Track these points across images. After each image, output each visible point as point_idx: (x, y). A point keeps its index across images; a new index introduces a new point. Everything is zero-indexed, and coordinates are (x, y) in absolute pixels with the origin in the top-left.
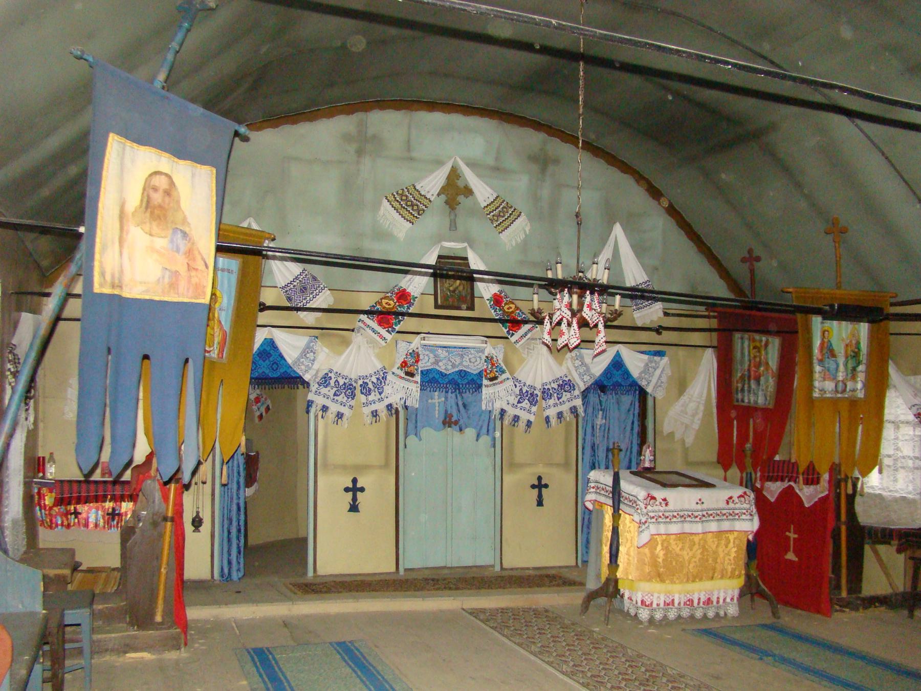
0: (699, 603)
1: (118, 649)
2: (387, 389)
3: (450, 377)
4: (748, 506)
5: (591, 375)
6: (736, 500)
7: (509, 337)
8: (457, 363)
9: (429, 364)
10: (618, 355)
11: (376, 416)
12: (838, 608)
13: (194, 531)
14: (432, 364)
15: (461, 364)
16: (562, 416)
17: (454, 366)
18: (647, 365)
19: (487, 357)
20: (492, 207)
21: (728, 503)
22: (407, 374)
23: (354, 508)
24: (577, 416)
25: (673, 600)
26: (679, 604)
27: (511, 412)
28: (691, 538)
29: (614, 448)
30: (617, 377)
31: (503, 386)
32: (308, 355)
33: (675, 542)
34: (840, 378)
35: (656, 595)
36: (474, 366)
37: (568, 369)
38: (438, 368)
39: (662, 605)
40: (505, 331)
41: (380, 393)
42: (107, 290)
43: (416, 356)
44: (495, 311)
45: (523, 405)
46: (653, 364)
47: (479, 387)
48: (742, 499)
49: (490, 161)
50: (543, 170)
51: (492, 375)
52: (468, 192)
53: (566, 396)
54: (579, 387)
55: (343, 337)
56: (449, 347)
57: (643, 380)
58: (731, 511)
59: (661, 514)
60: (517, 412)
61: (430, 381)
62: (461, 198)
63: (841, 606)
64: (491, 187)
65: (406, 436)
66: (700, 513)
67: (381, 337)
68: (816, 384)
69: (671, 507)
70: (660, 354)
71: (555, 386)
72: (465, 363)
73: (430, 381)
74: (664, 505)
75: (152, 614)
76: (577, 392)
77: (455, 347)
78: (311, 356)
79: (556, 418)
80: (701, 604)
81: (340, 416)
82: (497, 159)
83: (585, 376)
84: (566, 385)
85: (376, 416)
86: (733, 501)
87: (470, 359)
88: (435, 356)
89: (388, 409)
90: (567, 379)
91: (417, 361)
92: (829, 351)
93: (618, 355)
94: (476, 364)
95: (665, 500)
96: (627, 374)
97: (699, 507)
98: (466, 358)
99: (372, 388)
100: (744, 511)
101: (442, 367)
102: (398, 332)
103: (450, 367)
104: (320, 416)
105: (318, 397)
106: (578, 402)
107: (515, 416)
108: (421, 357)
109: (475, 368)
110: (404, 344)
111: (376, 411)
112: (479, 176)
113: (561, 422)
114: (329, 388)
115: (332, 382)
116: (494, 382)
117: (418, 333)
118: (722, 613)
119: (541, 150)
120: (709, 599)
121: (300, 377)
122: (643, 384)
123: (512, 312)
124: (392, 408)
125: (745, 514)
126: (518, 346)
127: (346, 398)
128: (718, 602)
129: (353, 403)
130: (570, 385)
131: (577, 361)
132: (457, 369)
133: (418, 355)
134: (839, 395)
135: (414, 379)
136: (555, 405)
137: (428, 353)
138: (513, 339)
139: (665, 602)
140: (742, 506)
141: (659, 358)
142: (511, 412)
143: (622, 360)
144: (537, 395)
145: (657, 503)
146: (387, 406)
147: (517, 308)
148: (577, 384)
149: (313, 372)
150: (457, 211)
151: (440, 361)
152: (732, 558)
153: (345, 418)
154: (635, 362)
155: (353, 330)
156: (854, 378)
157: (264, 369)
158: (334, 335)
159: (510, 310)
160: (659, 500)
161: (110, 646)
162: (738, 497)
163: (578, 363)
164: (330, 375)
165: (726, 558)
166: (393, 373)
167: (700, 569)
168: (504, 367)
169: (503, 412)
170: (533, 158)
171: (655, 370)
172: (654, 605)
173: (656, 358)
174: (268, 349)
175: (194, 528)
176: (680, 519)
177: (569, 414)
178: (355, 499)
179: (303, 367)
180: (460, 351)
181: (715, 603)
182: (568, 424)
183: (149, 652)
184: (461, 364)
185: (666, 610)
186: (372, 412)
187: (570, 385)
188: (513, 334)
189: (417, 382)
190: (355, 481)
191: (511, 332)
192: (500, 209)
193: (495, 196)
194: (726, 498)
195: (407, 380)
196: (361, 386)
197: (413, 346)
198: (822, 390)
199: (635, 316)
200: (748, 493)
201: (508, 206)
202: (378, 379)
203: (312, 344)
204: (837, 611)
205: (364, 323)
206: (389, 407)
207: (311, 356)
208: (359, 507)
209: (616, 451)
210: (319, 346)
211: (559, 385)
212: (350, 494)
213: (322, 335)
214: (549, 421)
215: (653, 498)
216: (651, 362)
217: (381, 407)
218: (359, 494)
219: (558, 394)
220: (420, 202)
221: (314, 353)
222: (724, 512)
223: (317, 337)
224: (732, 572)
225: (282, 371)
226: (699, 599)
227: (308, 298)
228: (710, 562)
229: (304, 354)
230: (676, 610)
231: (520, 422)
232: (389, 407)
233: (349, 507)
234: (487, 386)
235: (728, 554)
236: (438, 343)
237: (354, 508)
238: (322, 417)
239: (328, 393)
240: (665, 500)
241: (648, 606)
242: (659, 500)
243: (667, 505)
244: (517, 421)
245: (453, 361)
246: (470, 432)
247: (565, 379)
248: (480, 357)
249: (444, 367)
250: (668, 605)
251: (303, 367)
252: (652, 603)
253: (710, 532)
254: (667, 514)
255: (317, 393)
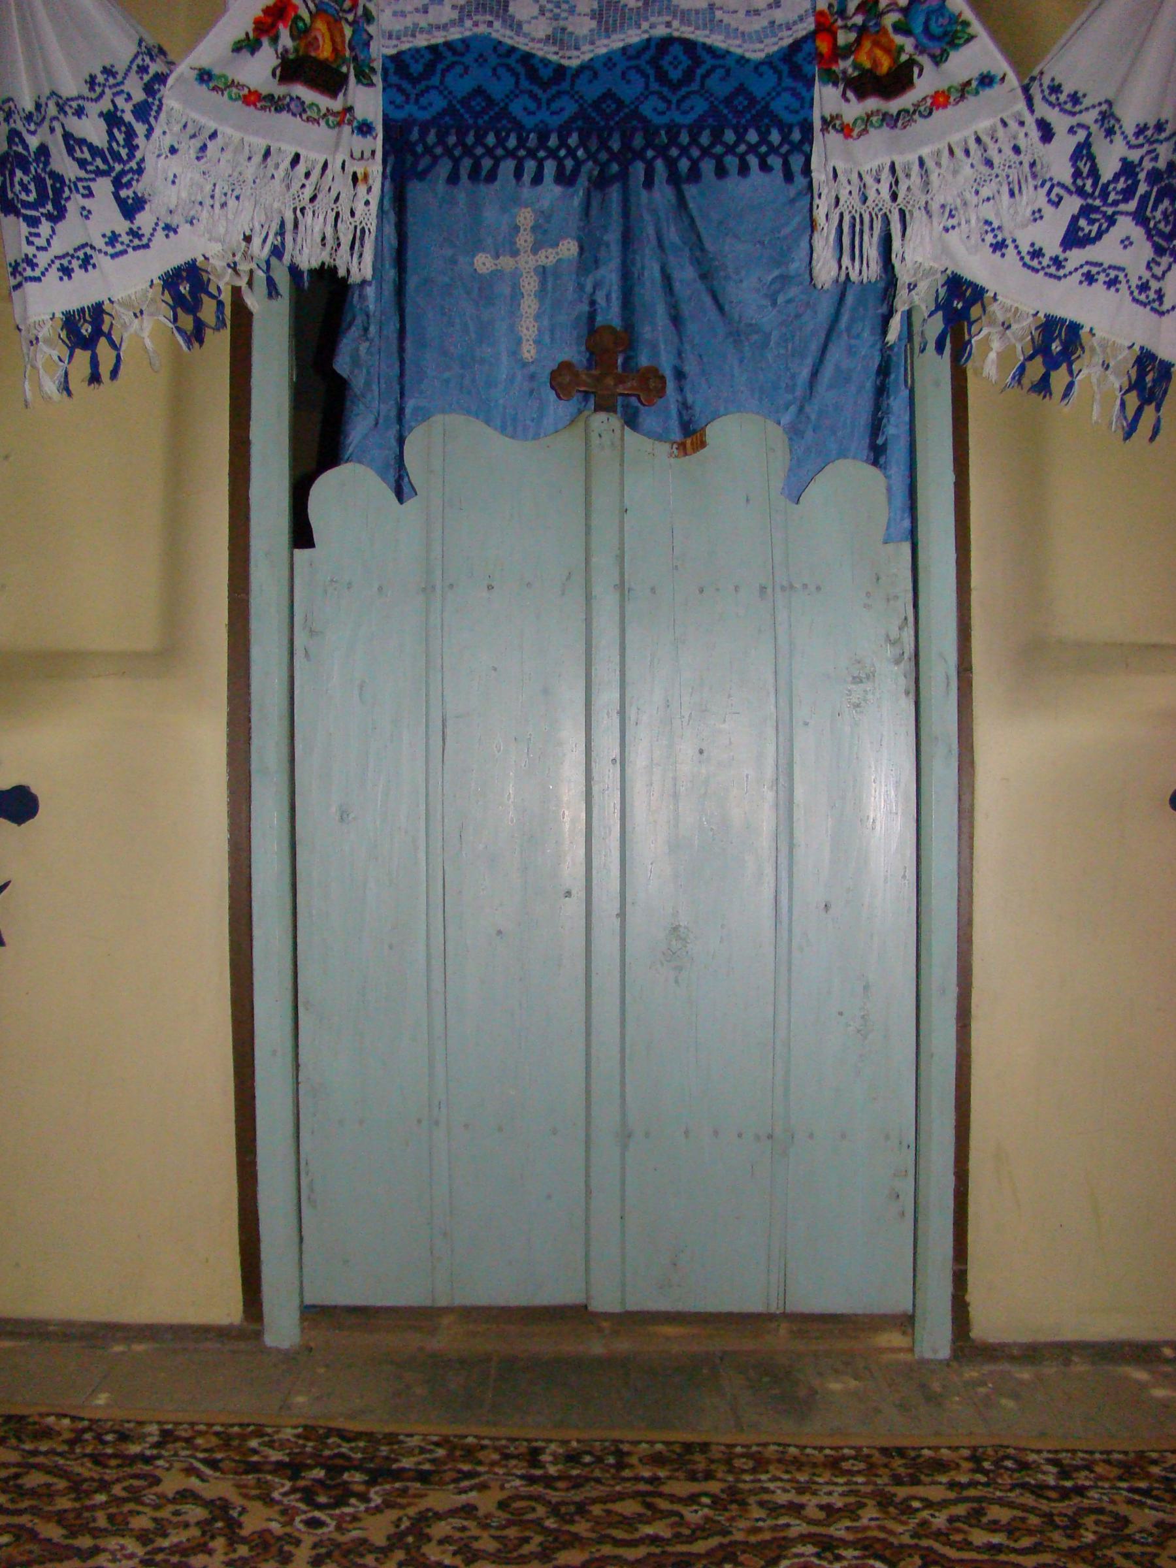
3: (591, 91)
11: (88, 344)
38: (500, 32)
41: (130, 208)
45: (1106, 251)
85: (88, 344)
89: (179, 302)
103: (583, 26)
114: (75, 203)
202: (112, 119)
231: (1088, 370)
249: (542, 28)
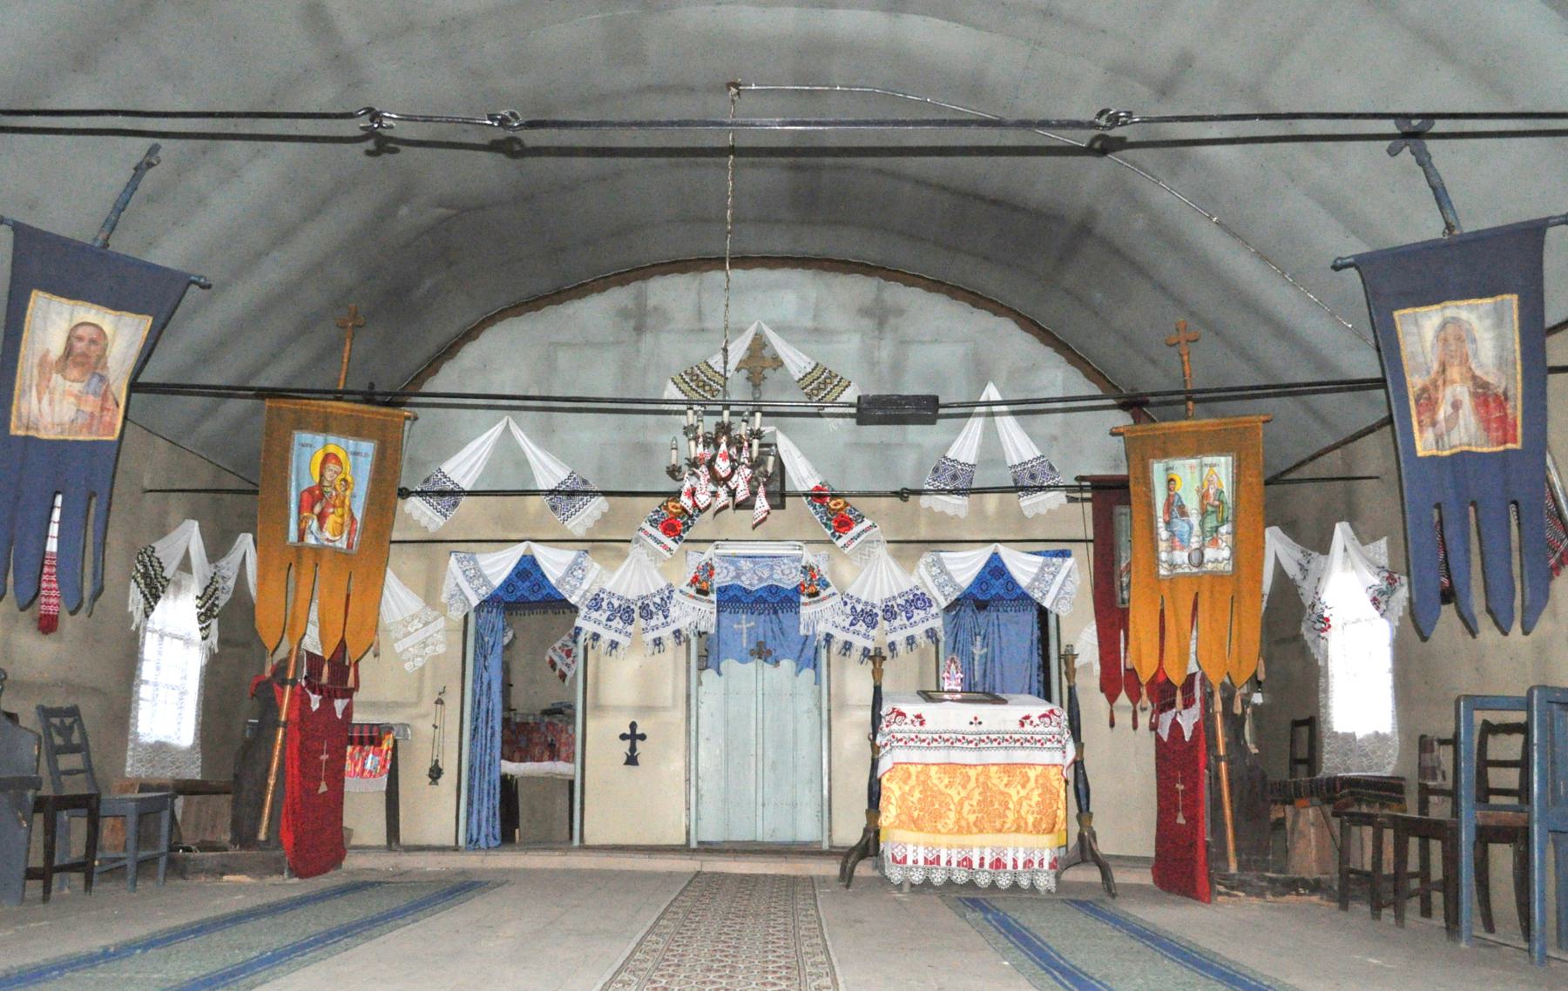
0: (982, 865)
1: (214, 870)
2: (674, 612)
4: (1056, 730)
5: (955, 586)
6: (1037, 721)
7: (834, 540)
8: (765, 577)
9: (728, 578)
10: (995, 556)
11: (659, 645)
12: (1221, 888)
13: (430, 784)
14: (733, 578)
15: (771, 577)
16: (913, 642)
17: (761, 579)
18: (1042, 569)
19: (805, 567)
20: (809, 379)
21: (1022, 724)
22: (699, 591)
23: (632, 760)
24: (937, 642)
25: (938, 857)
26: (949, 862)
27: (840, 637)
28: (964, 771)
29: (875, 655)
30: (997, 587)
31: (828, 604)
32: (575, 573)
33: (938, 775)
34: (1195, 546)
35: (910, 848)
36: (789, 578)
37: (921, 578)
39: (921, 863)
40: (829, 533)
41: (666, 617)
42: (21, 433)
43: (709, 569)
44: (815, 508)
45: (857, 627)
46: (1052, 569)
47: (798, 604)
48: (1047, 720)
49: (808, 323)
50: (881, 324)
51: (812, 590)
52: (778, 363)
53: (918, 615)
54: (938, 604)
55: (619, 550)
56: (755, 557)
57: (1036, 591)
58: (1029, 737)
59: (913, 736)
60: (849, 637)
61: (730, 600)
62: (768, 372)
63: (1226, 887)
64: (808, 355)
65: (701, 669)
66: (977, 737)
67: (665, 547)
68: (1163, 556)
69: (928, 726)
70: (1065, 554)
71: (901, 601)
72: (775, 576)
73: (730, 600)
74: (917, 724)
75: (256, 831)
76: (934, 610)
77: (762, 557)
78: (579, 573)
79: (904, 644)
80: (987, 867)
81: (614, 645)
82: (815, 317)
83: (947, 588)
84: (919, 600)
85: (659, 645)
86: (1032, 722)
87: (782, 571)
88: (737, 569)
90: (918, 592)
91: (711, 575)
92: (1175, 507)
93: (995, 556)
94: (790, 577)
95: (919, 717)
96: (1011, 582)
97: (973, 728)
98: (778, 570)
99: (654, 610)
100: (1050, 737)
101: (745, 582)
102: (686, 541)
103: (756, 582)
104: (590, 647)
105: (586, 623)
106: (937, 624)
107: (846, 642)
108: (717, 570)
109: (789, 582)
110: (696, 555)
111: (660, 638)
112: (789, 341)
113: (912, 650)
114: (600, 612)
115: (604, 605)
116: (816, 599)
117: (713, 541)
118: (1024, 883)
119: (876, 300)
120: (998, 860)
121: (566, 600)
122: (1036, 596)
123: (841, 509)
124: (680, 634)
125: (1050, 740)
126: (847, 551)
127: (622, 624)
128: (1015, 866)
129: (630, 629)
130: (923, 600)
131: (934, 569)
132: (765, 584)
133: (712, 568)
134: (1195, 570)
135: (708, 598)
136: (903, 627)
137: (726, 565)
138: (840, 543)
139: (926, 859)
140: (1046, 730)
141: (1060, 560)
142: (840, 637)
143: (1004, 565)
144: (876, 614)
145: (908, 720)
146: (674, 633)
147: (847, 504)
148: (935, 598)
149: (579, 592)
150: (762, 388)
151: (744, 574)
152: (1033, 803)
153: (620, 648)
154: (1023, 567)
155: (630, 541)
156: (1215, 542)
157: (523, 592)
158: (605, 547)
159: (838, 507)
160: (910, 716)
161: (207, 866)
162: (1040, 717)
163: (935, 570)
164: (602, 595)
165: (1024, 804)
166: (681, 591)
167: (980, 815)
168: (828, 579)
169: (829, 638)
170: (864, 312)
171: (1054, 576)
172: (909, 862)
173: (1054, 560)
174: (528, 567)
175: (430, 780)
176: (942, 744)
177: (925, 638)
178: (633, 748)
179: (568, 587)
180: (769, 562)
181: (1010, 867)
182: (923, 655)
183: (249, 876)
184: (771, 577)
185: (928, 871)
186: (655, 640)
187: (923, 600)
188: (840, 537)
189: (713, 602)
190: (633, 726)
191: (837, 534)
192: (820, 380)
193: (813, 365)
194: (1020, 717)
195: (700, 600)
196: (640, 608)
197: (704, 558)
198: (1173, 566)
199: (1022, 504)
200: (1057, 712)
201: (832, 376)
202: (662, 599)
203: (580, 560)
204: (1220, 894)
205: (646, 533)
206: (677, 633)
207: (579, 573)
208: (639, 759)
209: (878, 659)
210: (588, 561)
211: (907, 601)
212: (627, 743)
213: (594, 549)
214: (895, 649)
215: (903, 714)
216: (1047, 565)
217: (666, 633)
218: (639, 743)
219: (907, 612)
220: (714, 381)
221: (583, 570)
222: (1016, 737)
223: (586, 551)
224: (1034, 825)
225: (545, 592)
226: (982, 859)
227: (577, 506)
228: (996, 806)
229: (570, 571)
230: (943, 872)
231: (853, 650)
232: (677, 633)
233: (625, 758)
234: (806, 604)
235: (1028, 797)
236: (737, 552)
237: (632, 760)
238: (593, 647)
239: (599, 618)
240: (919, 717)
241: (899, 863)
242: (910, 716)
243: (922, 723)
244: (849, 649)
245: (760, 574)
246: (787, 665)
247: (916, 592)
248: (796, 568)
250: (932, 863)
251: (568, 587)
252: (905, 858)
253: (993, 764)
254: (923, 736)
255: (587, 618)
